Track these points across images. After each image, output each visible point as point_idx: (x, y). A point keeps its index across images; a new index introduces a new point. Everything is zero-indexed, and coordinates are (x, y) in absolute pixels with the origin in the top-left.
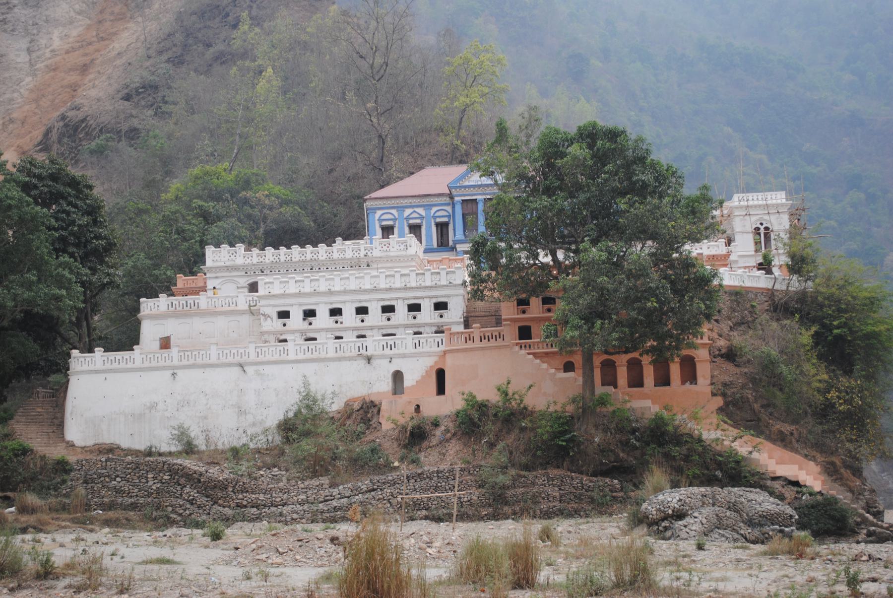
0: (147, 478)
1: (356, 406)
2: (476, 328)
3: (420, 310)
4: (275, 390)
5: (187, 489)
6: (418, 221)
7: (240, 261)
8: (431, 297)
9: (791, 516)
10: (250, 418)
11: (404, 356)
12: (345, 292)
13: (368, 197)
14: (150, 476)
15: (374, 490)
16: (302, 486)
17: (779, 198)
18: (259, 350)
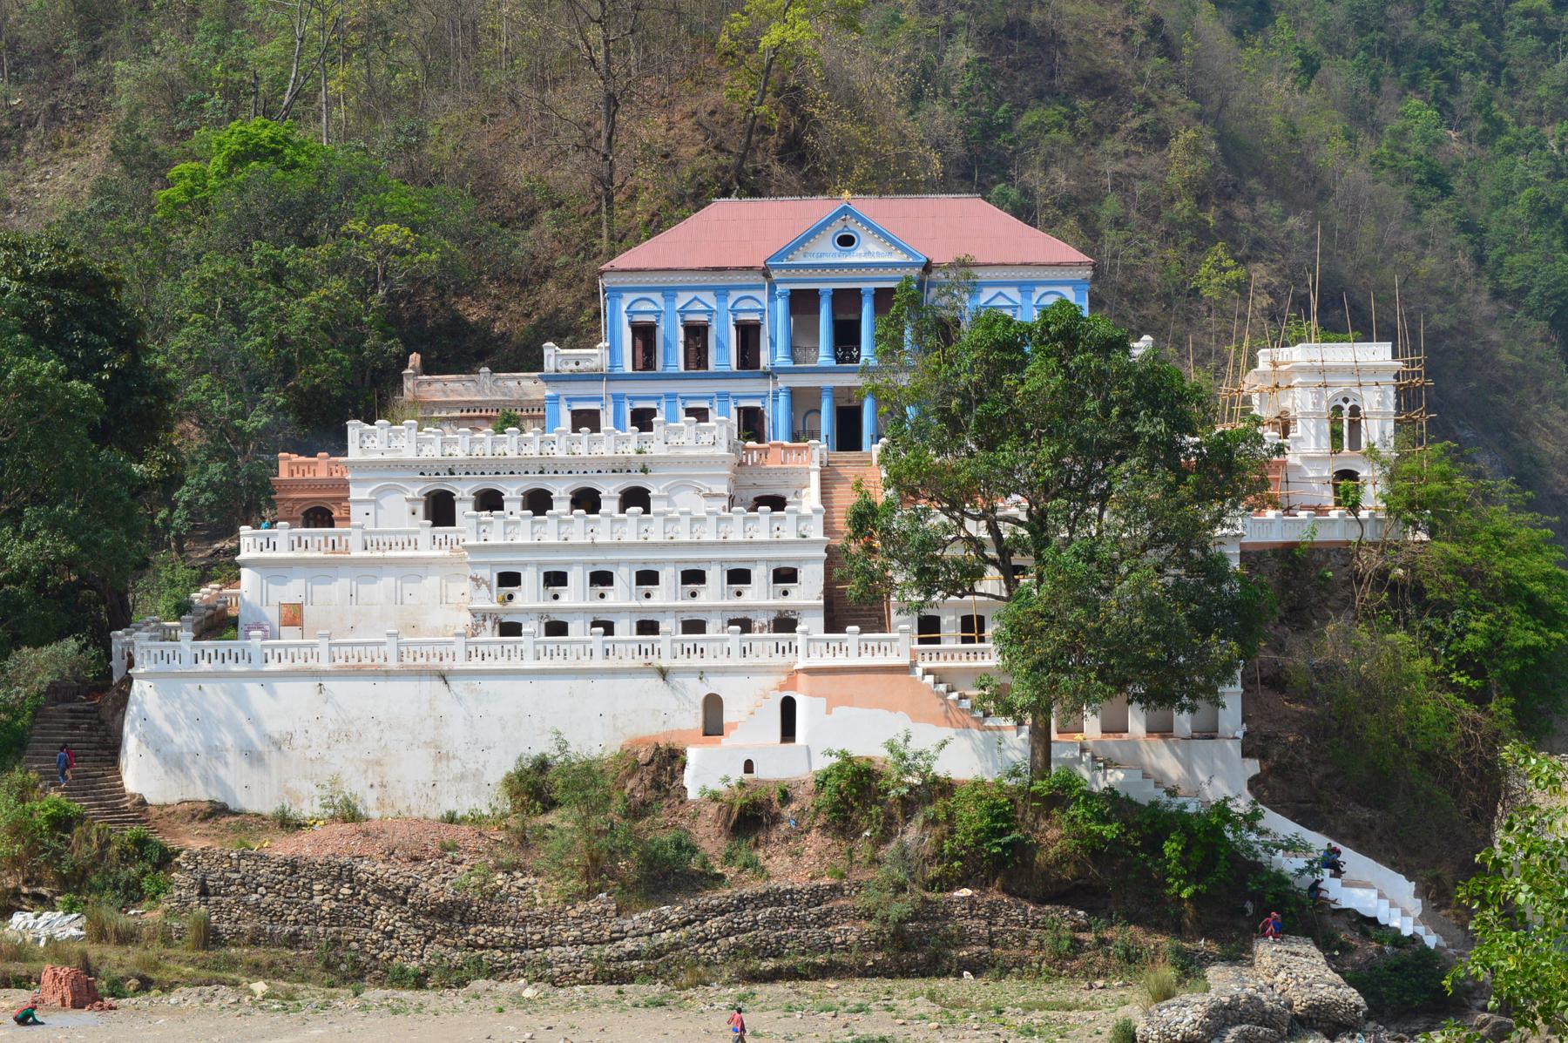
0: (311, 890)
1: (643, 757)
2: (852, 633)
3: (611, 583)
4: (501, 719)
5: (382, 913)
6: (704, 318)
7: (409, 454)
8: (768, 561)
9: (1357, 1007)
10: (456, 767)
11: (723, 671)
12: (619, 546)
13: (606, 266)
14: (317, 887)
15: (690, 922)
16: (573, 913)
17: (1379, 354)
18: (472, 648)
